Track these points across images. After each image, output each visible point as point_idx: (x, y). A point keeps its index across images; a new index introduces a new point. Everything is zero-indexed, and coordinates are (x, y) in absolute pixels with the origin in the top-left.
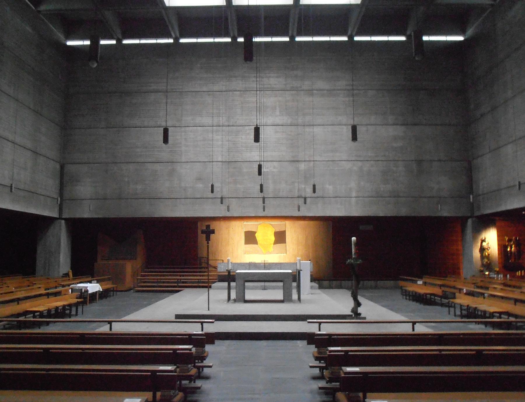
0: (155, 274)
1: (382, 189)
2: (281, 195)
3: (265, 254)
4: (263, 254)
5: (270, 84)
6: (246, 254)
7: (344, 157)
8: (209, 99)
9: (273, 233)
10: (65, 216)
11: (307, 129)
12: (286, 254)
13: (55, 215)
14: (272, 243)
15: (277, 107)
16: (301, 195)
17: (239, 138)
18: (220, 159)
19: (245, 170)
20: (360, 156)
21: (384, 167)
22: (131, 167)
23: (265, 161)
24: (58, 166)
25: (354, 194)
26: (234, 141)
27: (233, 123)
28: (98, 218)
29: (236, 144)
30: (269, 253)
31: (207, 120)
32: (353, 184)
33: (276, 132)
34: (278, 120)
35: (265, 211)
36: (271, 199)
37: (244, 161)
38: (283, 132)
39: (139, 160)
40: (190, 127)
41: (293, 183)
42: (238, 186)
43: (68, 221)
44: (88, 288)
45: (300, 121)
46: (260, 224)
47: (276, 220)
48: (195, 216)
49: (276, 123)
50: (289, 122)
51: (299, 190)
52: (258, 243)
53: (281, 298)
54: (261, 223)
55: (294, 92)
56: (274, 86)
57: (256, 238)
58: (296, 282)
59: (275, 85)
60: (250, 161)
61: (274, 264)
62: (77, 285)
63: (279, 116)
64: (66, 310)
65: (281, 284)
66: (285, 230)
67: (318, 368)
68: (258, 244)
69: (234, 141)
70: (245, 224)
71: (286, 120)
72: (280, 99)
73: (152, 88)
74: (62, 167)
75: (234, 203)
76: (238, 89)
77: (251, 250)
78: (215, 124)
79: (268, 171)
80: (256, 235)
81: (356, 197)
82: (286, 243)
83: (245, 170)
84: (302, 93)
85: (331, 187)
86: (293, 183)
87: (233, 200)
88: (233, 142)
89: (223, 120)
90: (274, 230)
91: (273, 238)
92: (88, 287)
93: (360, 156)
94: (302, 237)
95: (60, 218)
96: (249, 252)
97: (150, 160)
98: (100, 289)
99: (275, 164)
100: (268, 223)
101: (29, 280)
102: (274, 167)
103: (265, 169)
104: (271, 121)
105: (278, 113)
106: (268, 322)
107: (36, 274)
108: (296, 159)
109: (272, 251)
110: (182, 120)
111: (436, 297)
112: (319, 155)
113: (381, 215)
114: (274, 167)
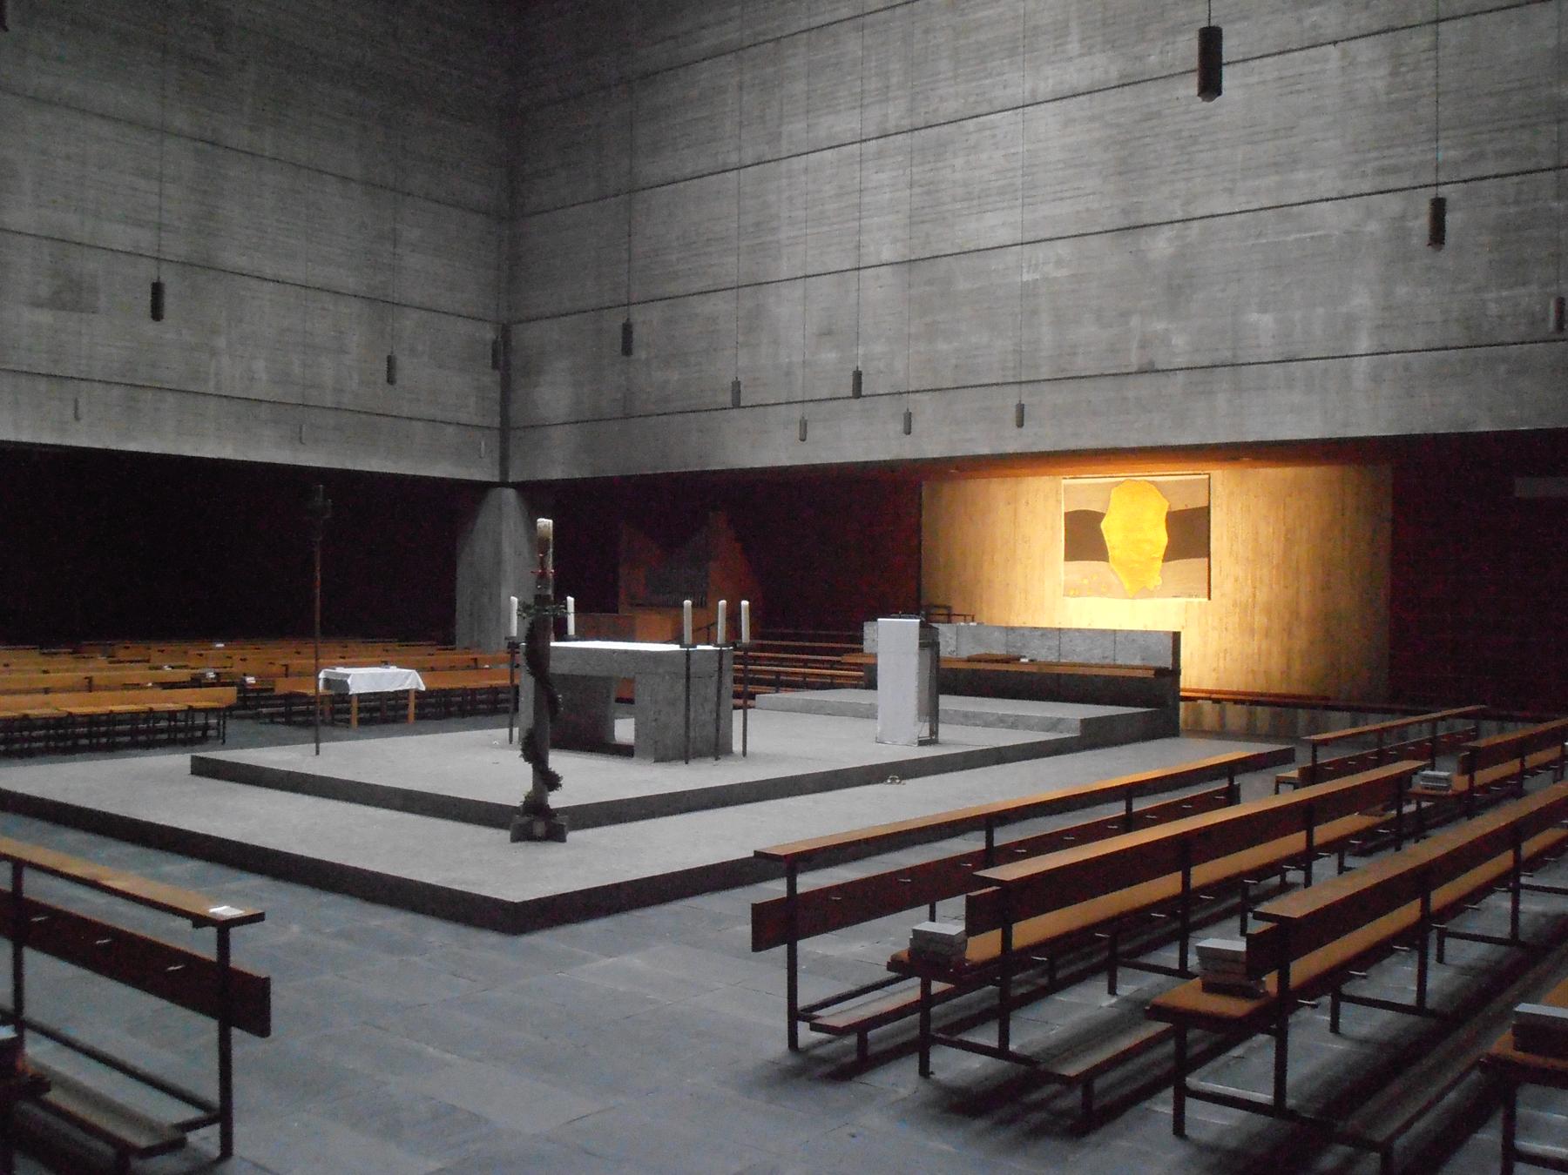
0: (770, 655)
1: (1493, 309)
3: (1134, 598)
4: (1128, 598)
6: (1068, 596)
7: (1329, 183)
8: (853, 45)
9: (1165, 514)
10: (513, 477)
12: (1206, 599)
13: (481, 471)
14: (1156, 556)
15: (1073, 24)
16: (1152, 363)
17: (945, 167)
18: (887, 254)
20: (1395, 170)
21: (1504, 203)
25: (1363, 344)
27: (927, 115)
29: (937, 191)
30: (1145, 593)
31: (845, 124)
32: (1361, 300)
33: (1069, 122)
34: (1074, 76)
35: (909, 433)
36: (1046, 387)
37: (959, 253)
38: (1092, 119)
39: (673, 288)
42: (942, 346)
43: (518, 486)
44: (349, 681)
46: (1117, 484)
47: (1168, 466)
49: (1066, 89)
50: (1114, 75)
51: (1143, 345)
52: (1110, 554)
54: (1123, 479)
57: (1101, 536)
60: (978, 250)
61: (1039, 633)
62: (334, 669)
63: (1081, 55)
65: (1182, 694)
66: (1202, 503)
68: (1108, 561)
70: (1067, 488)
71: (1103, 66)
73: (705, 44)
75: (926, 409)
77: (1086, 582)
78: (871, 130)
79: (1038, 277)
80: (1103, 525)
81: (1372, 354)
82: (1209, 556)
85: (1266, 321)
86: (1125, 315)
87: (926, 397)
88: (926, 189)
89: (895, 113)
90: (1167, 504)
91: (1162, 538)
92: (351, 678)
93: (1395, 170)
94: (1271, 530)
95: (504, 484)
96: (1073, 590)
97: (698, 286)
98: (418, 684)
99: (1062, 249)
100: (1146, 481)
101: (162, 651)
102: (1059, 263)
103: (1028, 272)
104: (1051, 81)
105: (1073, 47)
107: (457, 643)
108: (1134, 220)
109: (1156, 587)
110: (780, 133)
112: (1225, 190)
113: (1484, 426)
114: (1059, 263)
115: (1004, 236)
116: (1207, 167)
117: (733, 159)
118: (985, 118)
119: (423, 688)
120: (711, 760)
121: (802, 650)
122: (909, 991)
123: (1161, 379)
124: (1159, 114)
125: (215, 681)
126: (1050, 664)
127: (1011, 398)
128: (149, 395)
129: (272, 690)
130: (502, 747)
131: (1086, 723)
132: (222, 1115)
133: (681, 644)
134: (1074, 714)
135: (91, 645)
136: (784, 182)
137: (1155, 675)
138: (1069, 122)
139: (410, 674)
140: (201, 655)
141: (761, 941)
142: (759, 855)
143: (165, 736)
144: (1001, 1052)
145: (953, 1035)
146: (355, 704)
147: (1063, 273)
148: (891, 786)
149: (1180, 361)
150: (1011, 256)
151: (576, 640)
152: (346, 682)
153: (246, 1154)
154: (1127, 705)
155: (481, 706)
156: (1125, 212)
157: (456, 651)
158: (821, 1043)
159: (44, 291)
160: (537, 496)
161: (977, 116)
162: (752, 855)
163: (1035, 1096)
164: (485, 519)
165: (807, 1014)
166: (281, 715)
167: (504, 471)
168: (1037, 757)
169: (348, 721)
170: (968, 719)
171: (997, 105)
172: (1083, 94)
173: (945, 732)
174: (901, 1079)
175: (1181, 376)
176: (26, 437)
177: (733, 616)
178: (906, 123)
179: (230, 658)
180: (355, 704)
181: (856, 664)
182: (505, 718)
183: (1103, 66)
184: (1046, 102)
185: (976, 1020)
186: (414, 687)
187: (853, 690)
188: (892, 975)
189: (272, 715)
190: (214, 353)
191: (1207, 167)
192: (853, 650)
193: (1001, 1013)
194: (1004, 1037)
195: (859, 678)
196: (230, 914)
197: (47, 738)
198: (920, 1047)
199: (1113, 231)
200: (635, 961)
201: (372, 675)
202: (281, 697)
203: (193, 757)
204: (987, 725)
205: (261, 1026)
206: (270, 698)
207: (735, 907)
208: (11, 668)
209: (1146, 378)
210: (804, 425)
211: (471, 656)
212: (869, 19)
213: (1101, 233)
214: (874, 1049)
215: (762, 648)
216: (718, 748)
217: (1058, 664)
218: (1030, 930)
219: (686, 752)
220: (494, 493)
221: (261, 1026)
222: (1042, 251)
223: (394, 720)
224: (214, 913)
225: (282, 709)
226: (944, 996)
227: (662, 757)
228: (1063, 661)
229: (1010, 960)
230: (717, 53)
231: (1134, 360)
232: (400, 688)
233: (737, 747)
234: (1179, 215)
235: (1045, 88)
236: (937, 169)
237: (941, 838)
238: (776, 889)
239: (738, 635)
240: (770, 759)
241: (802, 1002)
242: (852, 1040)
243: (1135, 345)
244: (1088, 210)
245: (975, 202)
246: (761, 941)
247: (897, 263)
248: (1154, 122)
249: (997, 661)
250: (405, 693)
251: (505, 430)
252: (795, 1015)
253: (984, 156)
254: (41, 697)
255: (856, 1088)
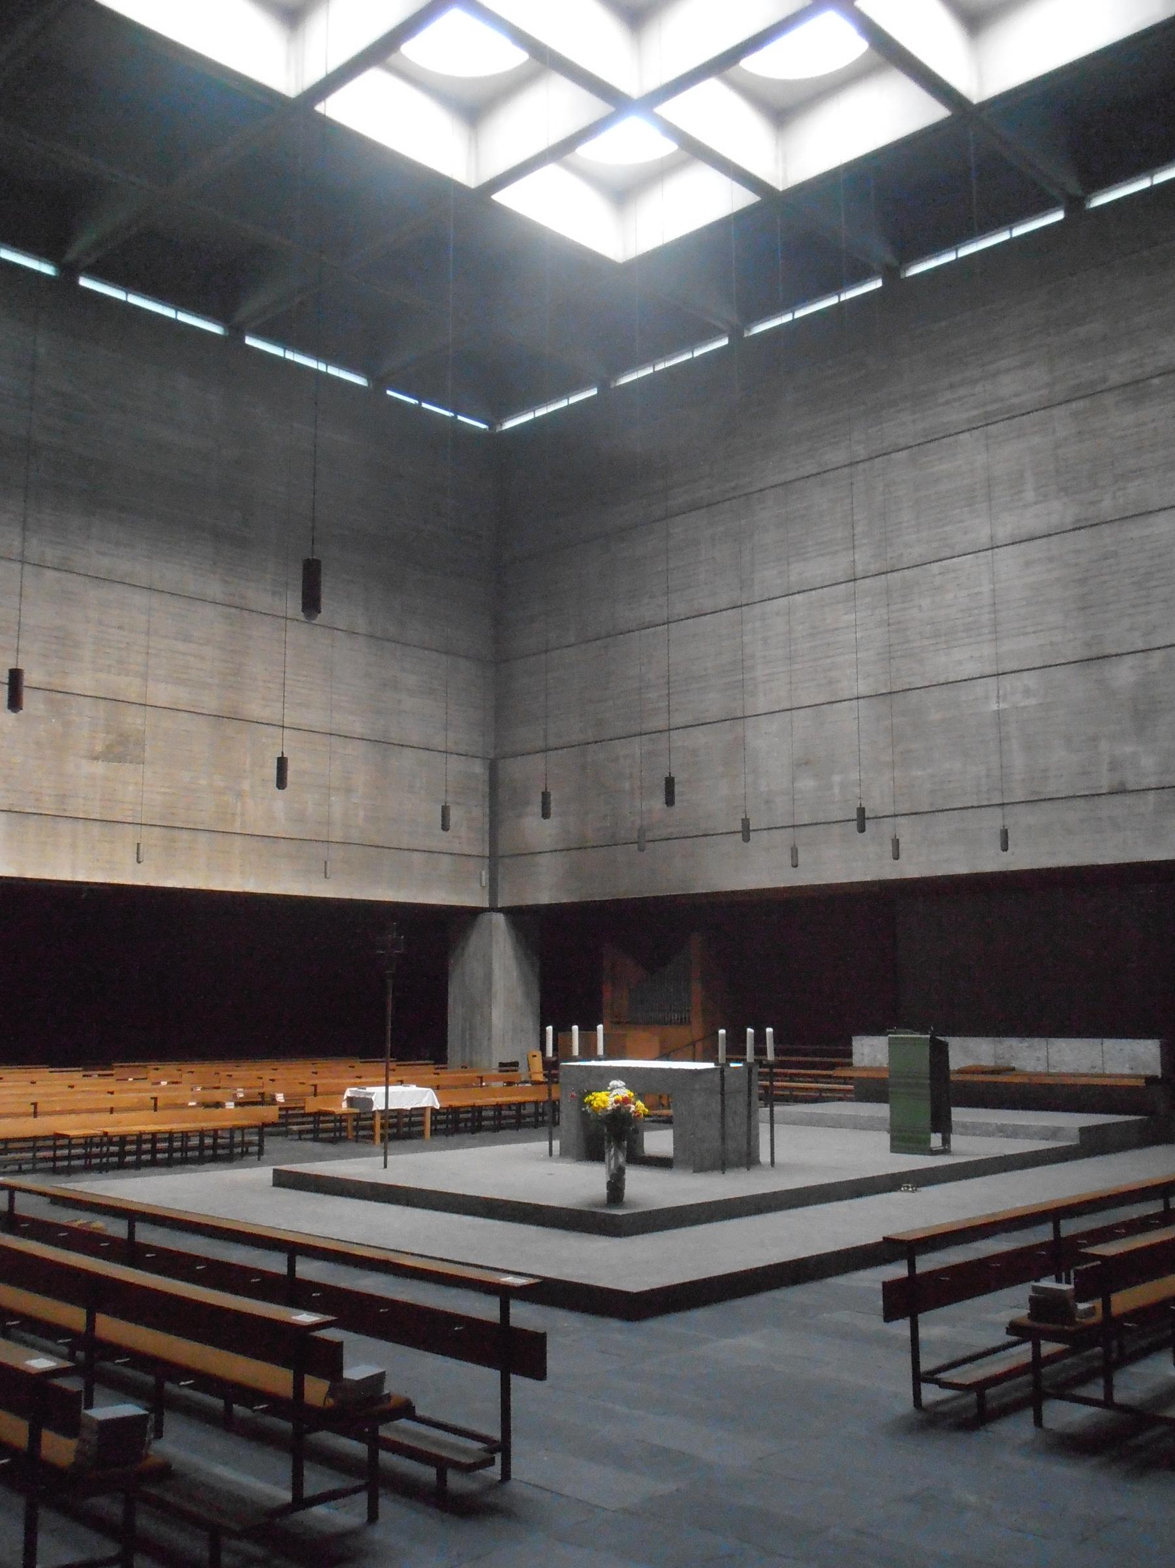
2: (1051, 789)
5: (1002, 400)
11: (1135, 531)
13: (472, 897)
16: (1122, 784)
17: (912, 607)
19: (935, 716)
22: (636, 747)
23: (861, 698)
24: (478, 768)
26: (899, 623)
28: (573, 903)
31: (817, 568)
33: (1028, 564)
34: (1031, 521)
38: (1051, 559)
40: (741, 606)
41: (1095, 739)
43: (510, 912)
44: (373, 1098)
45: (1107, 505)
48: (1101, 862)
50: (1069, 520)
51: (1114, 766)
53: (94, 1138)
55: (1081, 404)
56: (1015, 401)
58: (886, 1102)
59: (1016, 395)
64: (219, 1149)
65: (882, 1111)
67: (94, 1321)
69: (899, 623)
71: (1060, 511)
72: (1036, 440)
74: (493, 768)
76: (902, 442)
83: (935, 716)
84: (1109, 400)
86: (1095, 739)
89: (863, 559)
95: (493, 909)
98: (435, 1103)
99: (1029, 679)
101: (192, 1072)
102: (1027, 692)
105: (1030, 495)
106: (726, 1222)
108: (1095, 652)
111: (73, 1148)
114: (1027, 692)
115: (970, 669)
116: (1165, 601)
117: (709, 605)
118: (949, 561)
119: (438, 1106)
120: (744, 1170)
121: (813, 1066)
122: (1023, 1353)
123: (1128, 800)
124: (1115, 554)
125: (775, 1103)
126: (1039, 1074)
127: (993, 821)
128: (185, 835)
129: (303, 1108)
130: (544, 1160)
131: (1083, 1131)
132: (503, 1447)
133: (716, 1061)
134: (1072, 1122)
135: (130, 1066)
136: (758, 624)
137: (1146, 1082)
138: (1028, 564)
139: (427, 1091)
140: (230, 1076)
141: (890, 1314)
142: (887, 1240)
143: (81, 1162)
144: (1107, 1402)
145: (1063, 1392)
146: (378, 1121)
147: (1033, 701)
148: (911, 1194)
149: (1152, 781)
150: (979, 687)
151: (605, 1059)
152: (371, 1099)
153: (519, 1477)
154: (1119, 1113)
155: (528, 1120)
156: (1088, 645)
157: (448, 1070)
158: (954, 1398)
159: (99, 748)
160: (520, 917)
161: (940, 560)
162: (882, 1240)
163: (1141, 1439)
164: (475, 941)
165: (931, 1377)
166: (308, 1132)
167: (493, 893)
168: (967, 1177)
169: (372, 1138)
170: (971, 1130)
171: (957, 551)
172: (1040, 538)
173: (956, 1141)
174: (1020, 1427)
175: (1151, 796)
176: (81, 877)
177: (760, 1038)
178: (874, 567)
179: (261, 1078)
180: (378, 1121)
181: (845, 1078)
182: (544, 1130)
183: (1060, 511)
184: (1006, 545)
185: (1084, 1379)
186: (430, 1105)
187: (840, 1103)
188: (1014, 1338)
189: (300, 1132)
190: (240, 795)
191: (1165, 601)
192: (843, 1065)
193: (1107, 1371)
194: (1109, 1388)
195: (849, 1091)
196: (309, 1321)
197: (87, 1156)
198: (1035, 1401)
199: (1076, 662)
200: (751, 1341)
201: (422, 1091)
202: (309, 1115)
203: (275, 1170)
204: (989, 1134)
205: (538, 1371)
206: (303, 1115)
207: (873, 1279)
208: (75, 1089)
209: (1118, 799)
210: (794, 852)
211: (476, 1074)
212: (831, 475)
213: (1063, 664)
214: (992, 1405)
215: (781, 1065)
216: (749, 1160)
217: (1049, 1075)
218: (1124, 1301)
219: (722, 1164)
220: (485, 917)
221: (538, 1371)
222: (1008, 682)
223: (409, 1136)
224: (505, 1282)
225: (310, 1126)
226: (1053, 1358)
227: (700, 1168)
228: (1052, 1071)
229: (1111, 1325)
230: (694, 507)
231: (1105, 782)
232: (418, 1106)
233: (764, 1156)
234: (1140, 645)
235: (1003, 532)
236: (905, 609)
237: (974, 1239)
238: (898, 1271)
239: (764, 1052)
240: (801, 1168)
241: (926, 1365)
242: (973, 1397)
243: (1105, 767)
244: (1052, 644)
245: (943, 638)
246: (890, 1314)
247: (871, 696)
248: (1111, 561)
249: (984, 1073)
250: (420, 1111)
251: (494, 859)
252: (919, 1378)
253: (950, 596)
254: (107, 1117)
255: (978, 1438)
